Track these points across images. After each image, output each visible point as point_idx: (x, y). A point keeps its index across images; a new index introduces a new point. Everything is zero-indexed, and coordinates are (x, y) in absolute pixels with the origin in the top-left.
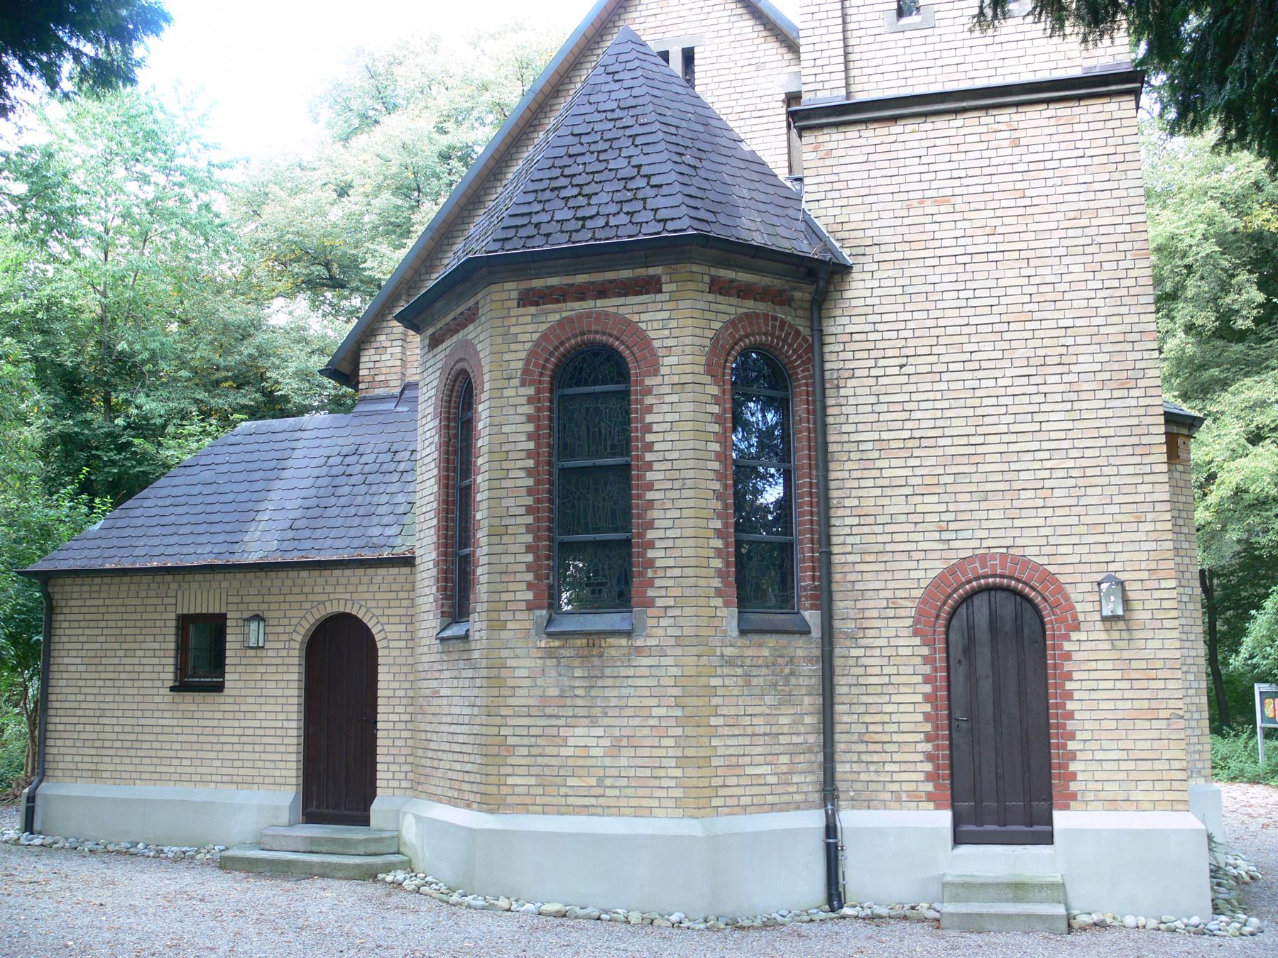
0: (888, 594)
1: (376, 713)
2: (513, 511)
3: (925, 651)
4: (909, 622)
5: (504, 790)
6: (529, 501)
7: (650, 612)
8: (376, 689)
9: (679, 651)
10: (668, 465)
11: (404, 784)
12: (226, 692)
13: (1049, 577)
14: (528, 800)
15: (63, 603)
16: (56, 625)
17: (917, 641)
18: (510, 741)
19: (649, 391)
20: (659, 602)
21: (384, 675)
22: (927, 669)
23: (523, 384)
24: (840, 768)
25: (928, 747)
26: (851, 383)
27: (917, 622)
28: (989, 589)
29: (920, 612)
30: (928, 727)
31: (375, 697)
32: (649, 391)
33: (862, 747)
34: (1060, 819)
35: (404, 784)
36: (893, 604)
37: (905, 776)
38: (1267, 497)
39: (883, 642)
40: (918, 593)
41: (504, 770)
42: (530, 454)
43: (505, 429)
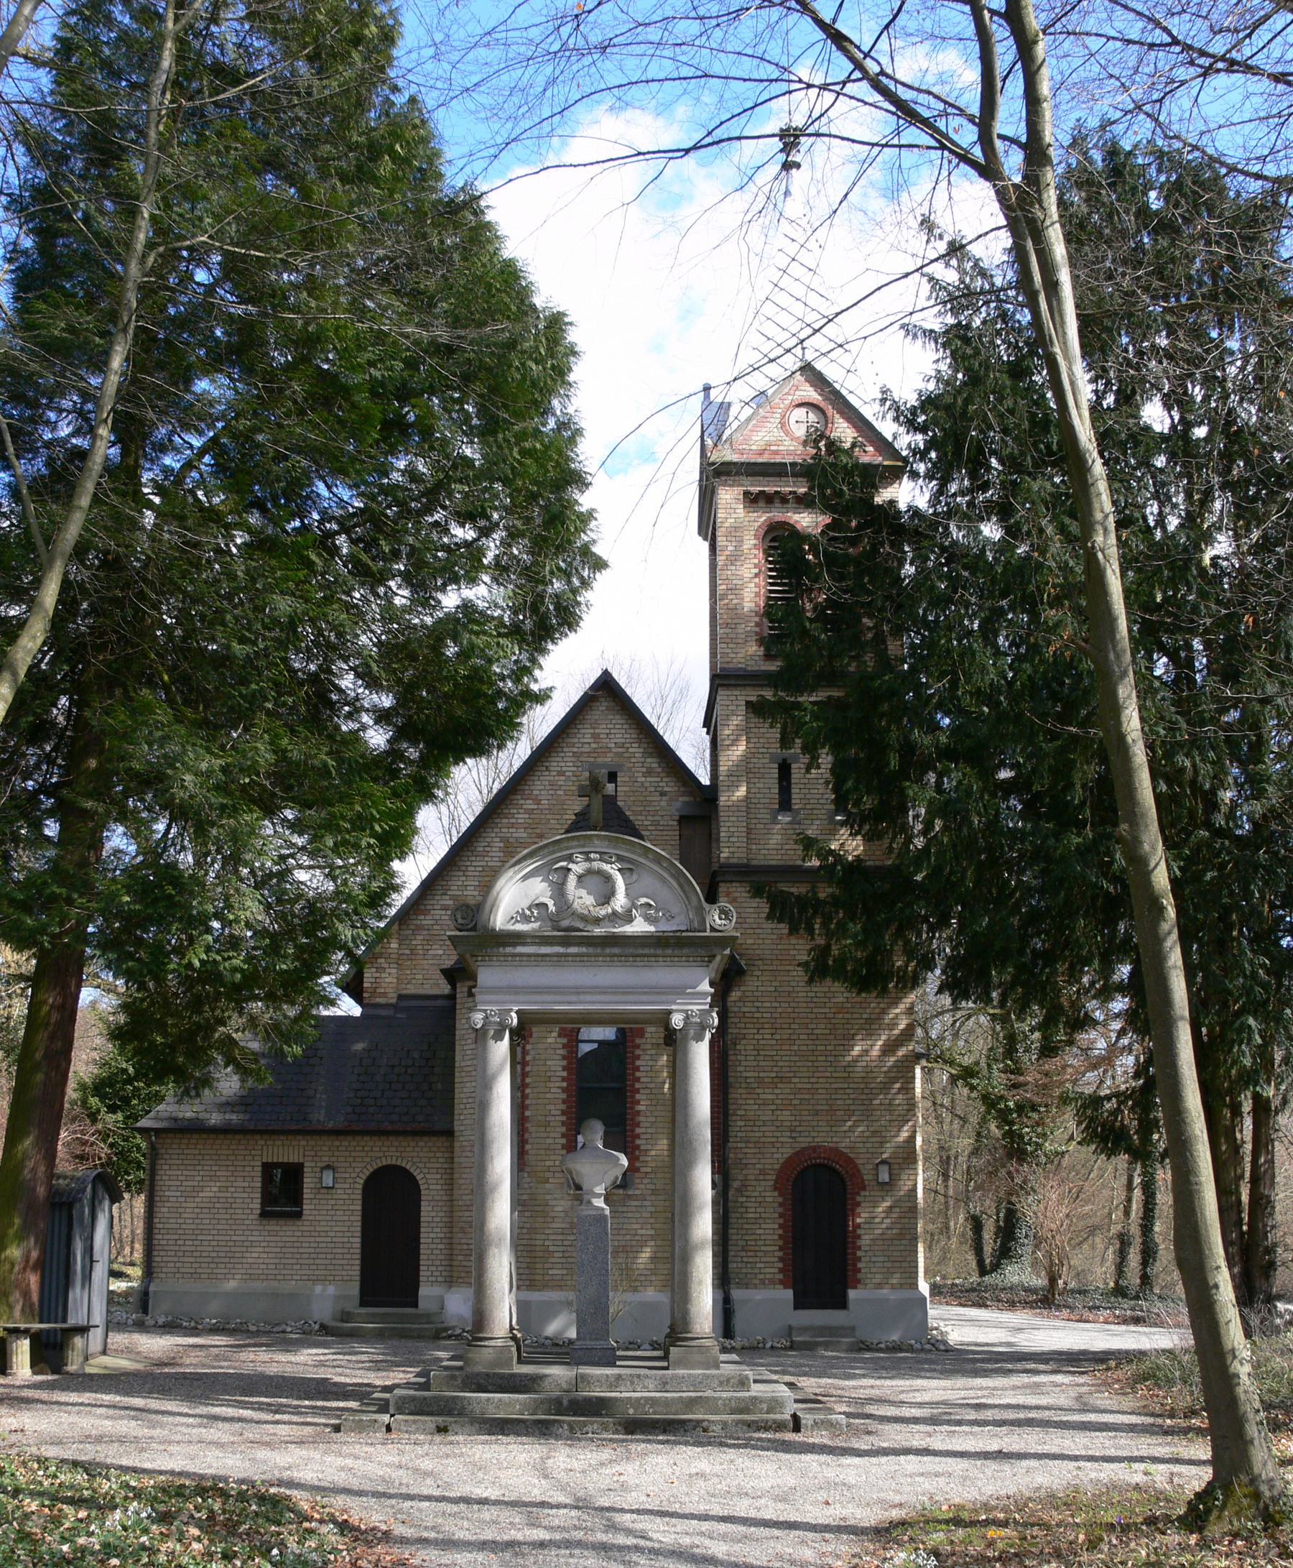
0: (760, 1166)
1: (419, 1233)
2: (553, 1112)
3: (780, 1200)
4: (771, 1183)
5: (547, 1278)
6: (563, 1107)
7: (637, 1175)
8: (419, 1216)
9: (654, 1198)
10: (648, 1091)
11: (440, 1279)
12: (304, 1217)
13: (850, 1161)
14: (562, 1283)
15: (163, 1151)
16: (158, 1167)
17: (776, 1194)
18: (551, 1248)
19: (638, 1047)
20: (643, 1170)
21: (425, 1207)
22: (781, 1210)
23: (560, 1036)
24: (730, 1265)
25: (780, 1254)
26: (743, 1042)
27: (776, 1182)
28: (815, 1165)
29: (779, 1178)
30: (781, 1243)
31: (419, 1222)
32: (638, 1047)
33: (744, 1254)
34: (852, 1294)
35: (440, 1279)
36: (763, 1172)
37: (768, 1270)
38: (992, 276)
39: (757, 1194)
40: (777, 1167)
41: (546, 1266)
42: (564, 1079)
43: (549, 1063)
